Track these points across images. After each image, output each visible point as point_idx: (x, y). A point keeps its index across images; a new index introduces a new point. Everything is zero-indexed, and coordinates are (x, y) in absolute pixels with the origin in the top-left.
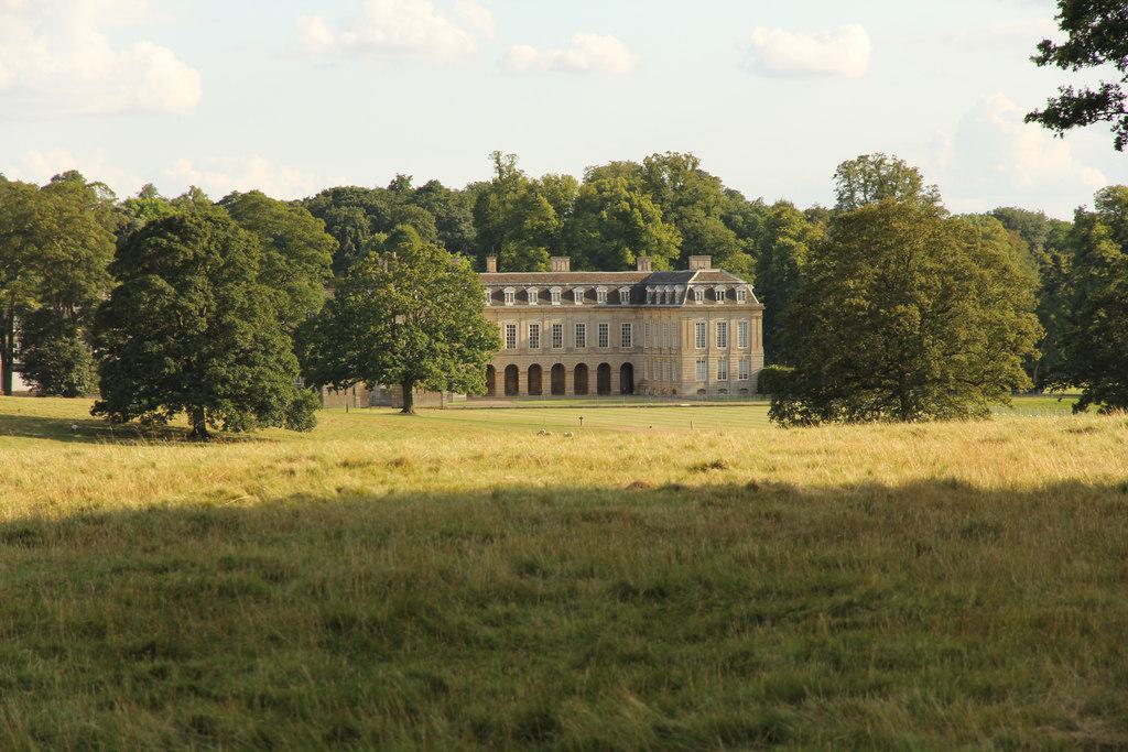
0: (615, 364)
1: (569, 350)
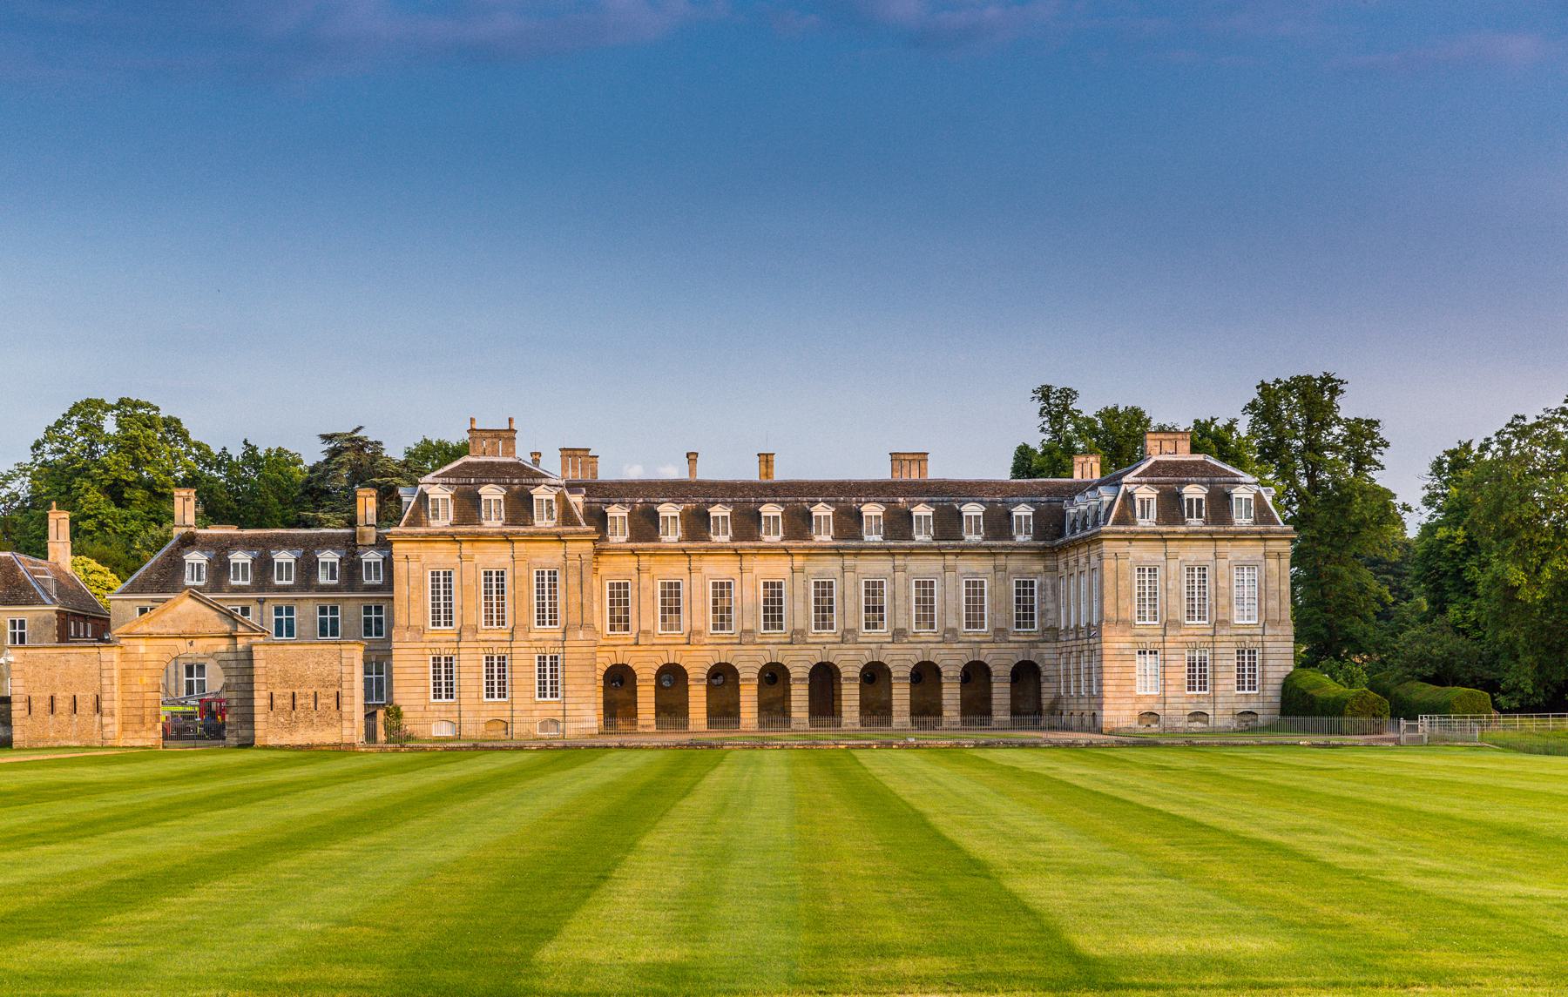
0: (1001, 663)
1: (899, 634)
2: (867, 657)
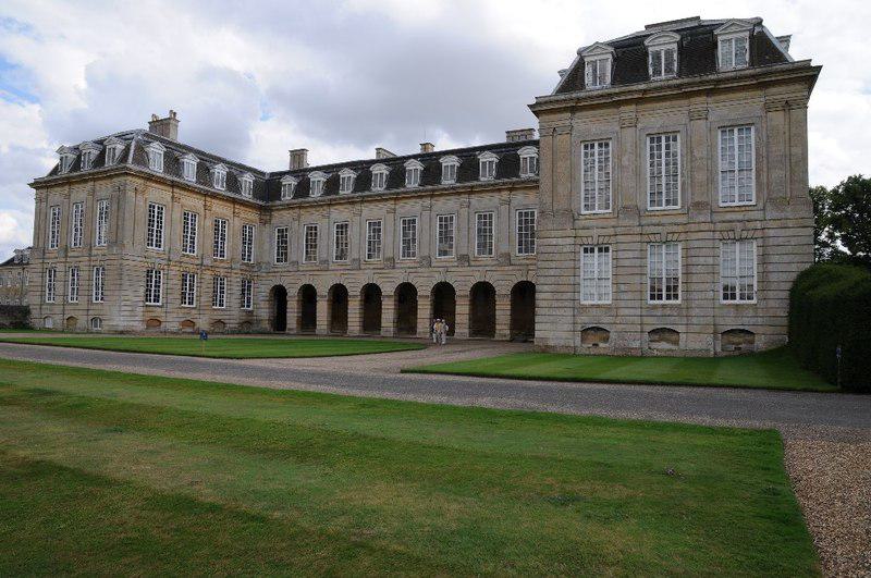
2: (438, 278)
